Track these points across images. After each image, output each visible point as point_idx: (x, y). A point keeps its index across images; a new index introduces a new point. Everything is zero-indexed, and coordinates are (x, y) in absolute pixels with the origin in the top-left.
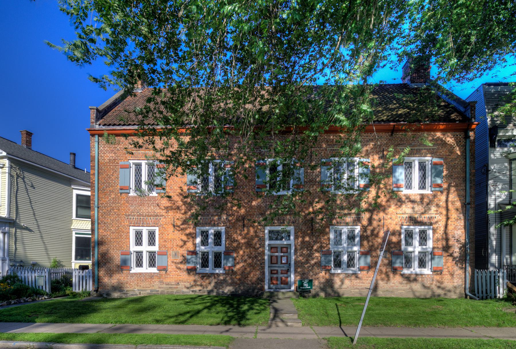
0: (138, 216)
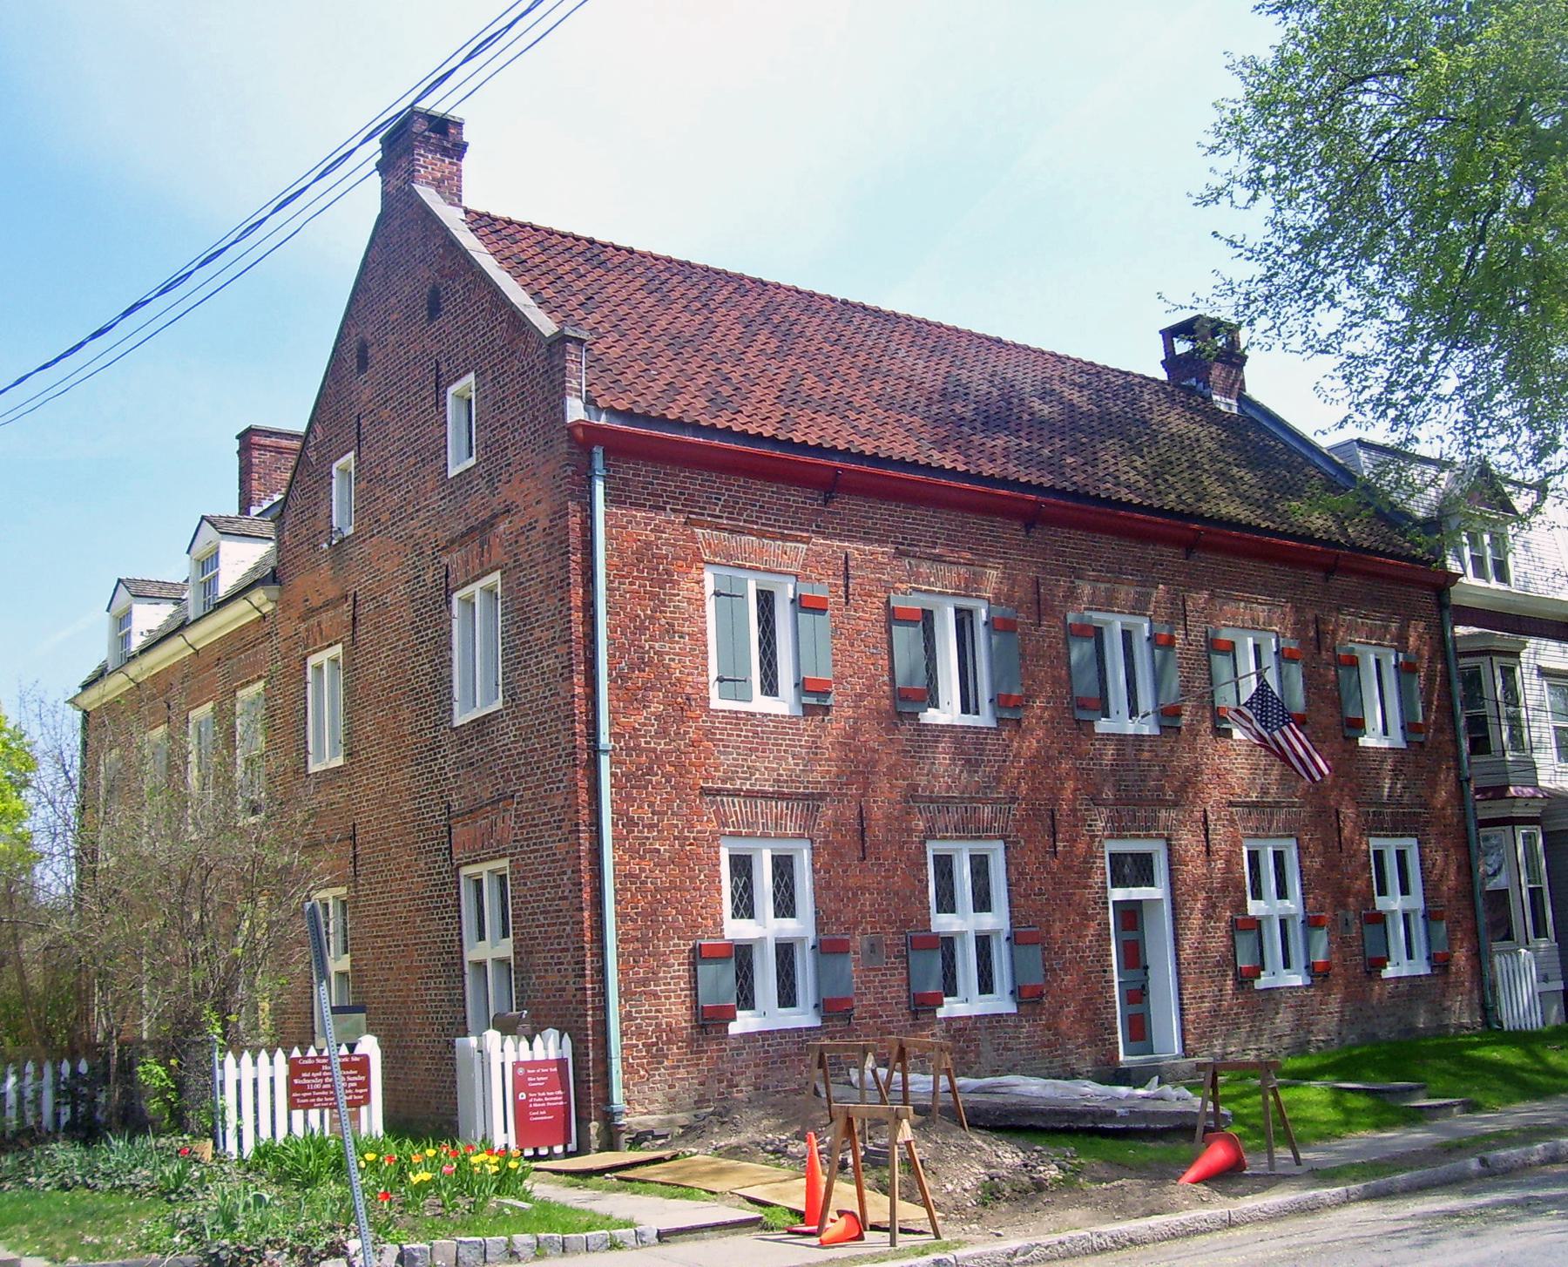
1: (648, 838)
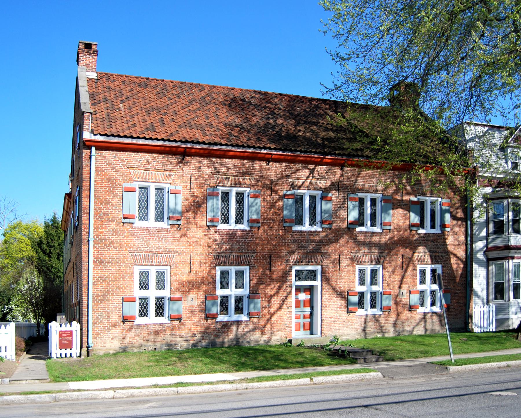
0: (146, 252)
1: (107, 266)
